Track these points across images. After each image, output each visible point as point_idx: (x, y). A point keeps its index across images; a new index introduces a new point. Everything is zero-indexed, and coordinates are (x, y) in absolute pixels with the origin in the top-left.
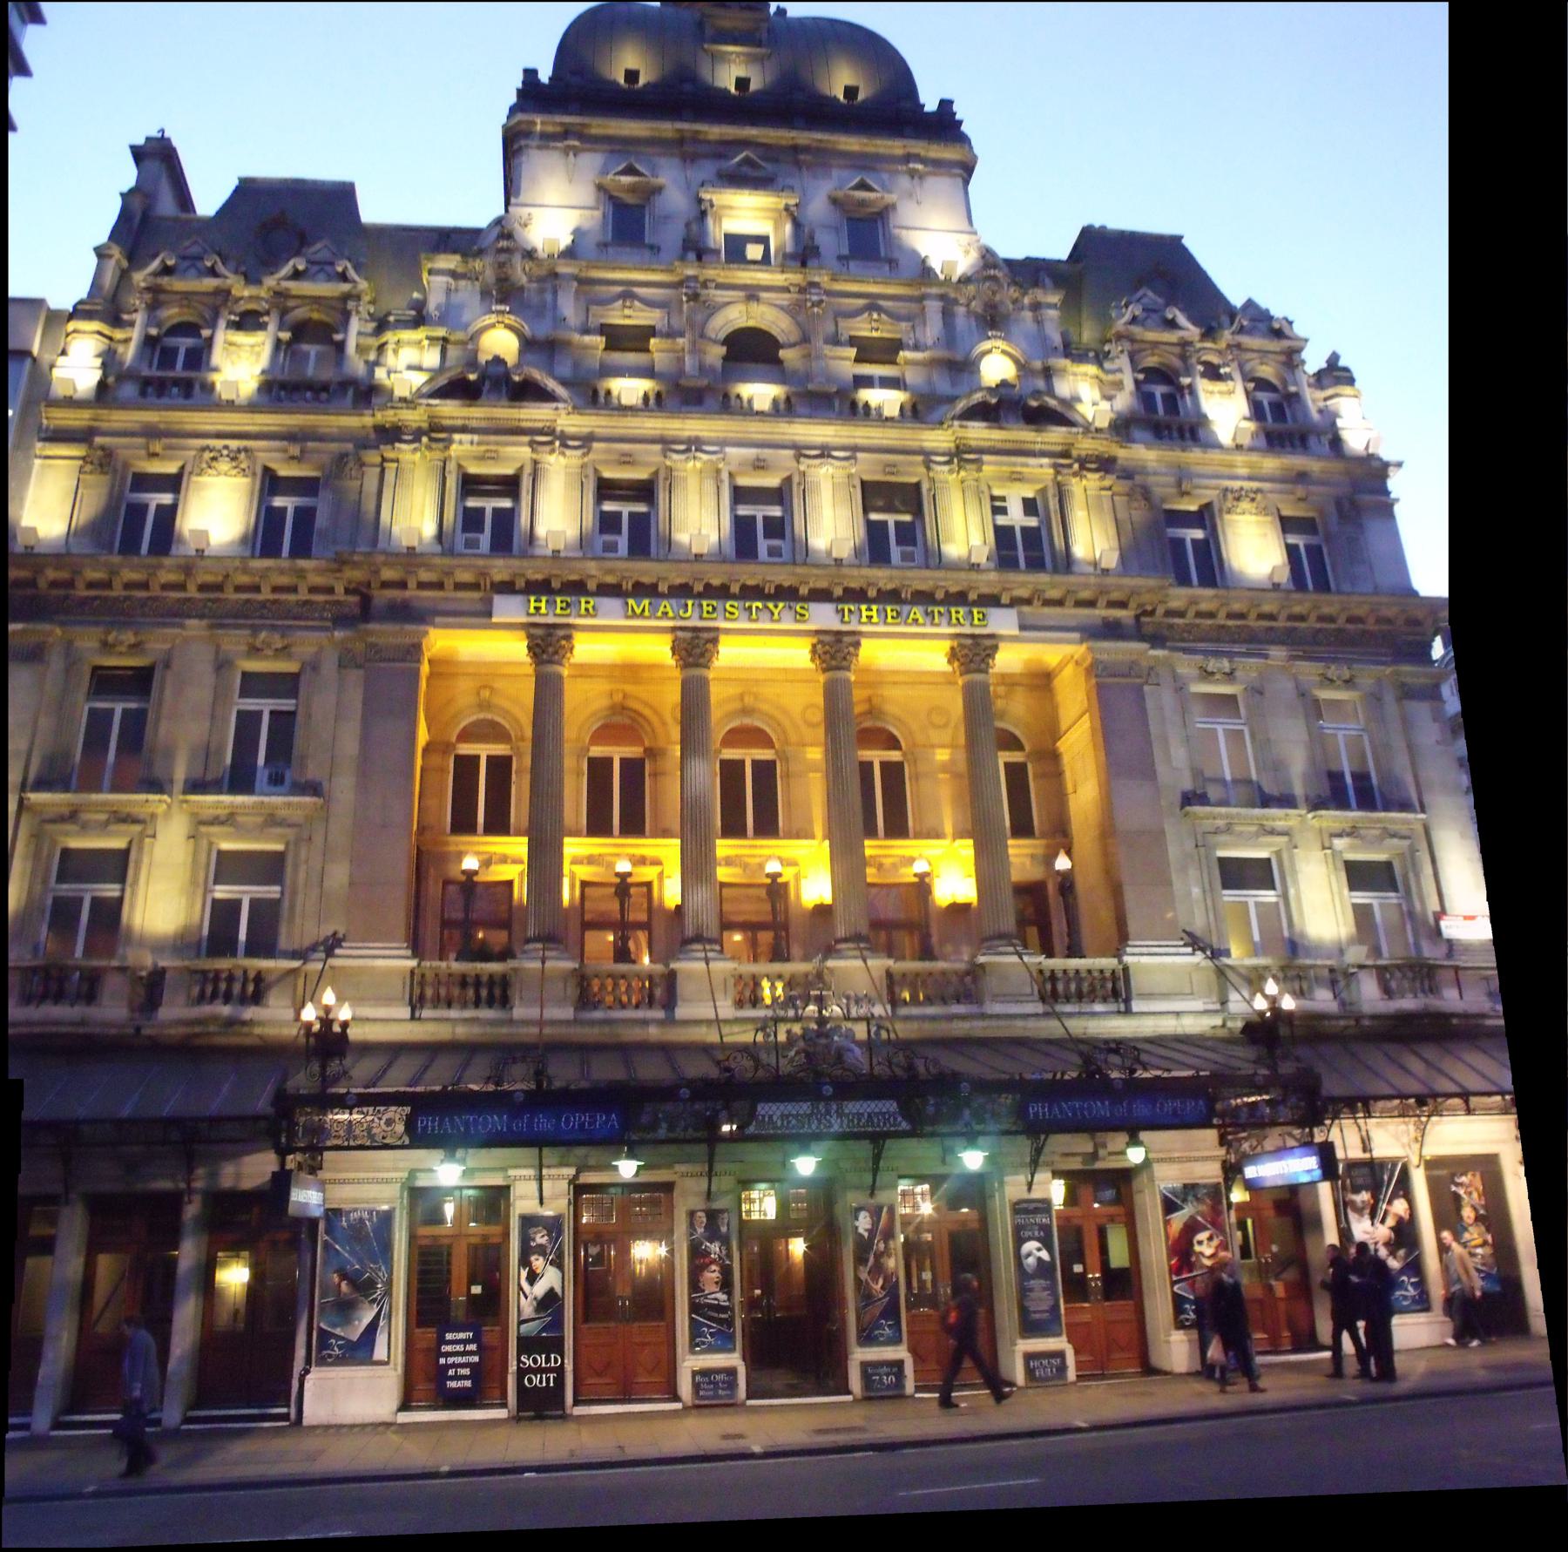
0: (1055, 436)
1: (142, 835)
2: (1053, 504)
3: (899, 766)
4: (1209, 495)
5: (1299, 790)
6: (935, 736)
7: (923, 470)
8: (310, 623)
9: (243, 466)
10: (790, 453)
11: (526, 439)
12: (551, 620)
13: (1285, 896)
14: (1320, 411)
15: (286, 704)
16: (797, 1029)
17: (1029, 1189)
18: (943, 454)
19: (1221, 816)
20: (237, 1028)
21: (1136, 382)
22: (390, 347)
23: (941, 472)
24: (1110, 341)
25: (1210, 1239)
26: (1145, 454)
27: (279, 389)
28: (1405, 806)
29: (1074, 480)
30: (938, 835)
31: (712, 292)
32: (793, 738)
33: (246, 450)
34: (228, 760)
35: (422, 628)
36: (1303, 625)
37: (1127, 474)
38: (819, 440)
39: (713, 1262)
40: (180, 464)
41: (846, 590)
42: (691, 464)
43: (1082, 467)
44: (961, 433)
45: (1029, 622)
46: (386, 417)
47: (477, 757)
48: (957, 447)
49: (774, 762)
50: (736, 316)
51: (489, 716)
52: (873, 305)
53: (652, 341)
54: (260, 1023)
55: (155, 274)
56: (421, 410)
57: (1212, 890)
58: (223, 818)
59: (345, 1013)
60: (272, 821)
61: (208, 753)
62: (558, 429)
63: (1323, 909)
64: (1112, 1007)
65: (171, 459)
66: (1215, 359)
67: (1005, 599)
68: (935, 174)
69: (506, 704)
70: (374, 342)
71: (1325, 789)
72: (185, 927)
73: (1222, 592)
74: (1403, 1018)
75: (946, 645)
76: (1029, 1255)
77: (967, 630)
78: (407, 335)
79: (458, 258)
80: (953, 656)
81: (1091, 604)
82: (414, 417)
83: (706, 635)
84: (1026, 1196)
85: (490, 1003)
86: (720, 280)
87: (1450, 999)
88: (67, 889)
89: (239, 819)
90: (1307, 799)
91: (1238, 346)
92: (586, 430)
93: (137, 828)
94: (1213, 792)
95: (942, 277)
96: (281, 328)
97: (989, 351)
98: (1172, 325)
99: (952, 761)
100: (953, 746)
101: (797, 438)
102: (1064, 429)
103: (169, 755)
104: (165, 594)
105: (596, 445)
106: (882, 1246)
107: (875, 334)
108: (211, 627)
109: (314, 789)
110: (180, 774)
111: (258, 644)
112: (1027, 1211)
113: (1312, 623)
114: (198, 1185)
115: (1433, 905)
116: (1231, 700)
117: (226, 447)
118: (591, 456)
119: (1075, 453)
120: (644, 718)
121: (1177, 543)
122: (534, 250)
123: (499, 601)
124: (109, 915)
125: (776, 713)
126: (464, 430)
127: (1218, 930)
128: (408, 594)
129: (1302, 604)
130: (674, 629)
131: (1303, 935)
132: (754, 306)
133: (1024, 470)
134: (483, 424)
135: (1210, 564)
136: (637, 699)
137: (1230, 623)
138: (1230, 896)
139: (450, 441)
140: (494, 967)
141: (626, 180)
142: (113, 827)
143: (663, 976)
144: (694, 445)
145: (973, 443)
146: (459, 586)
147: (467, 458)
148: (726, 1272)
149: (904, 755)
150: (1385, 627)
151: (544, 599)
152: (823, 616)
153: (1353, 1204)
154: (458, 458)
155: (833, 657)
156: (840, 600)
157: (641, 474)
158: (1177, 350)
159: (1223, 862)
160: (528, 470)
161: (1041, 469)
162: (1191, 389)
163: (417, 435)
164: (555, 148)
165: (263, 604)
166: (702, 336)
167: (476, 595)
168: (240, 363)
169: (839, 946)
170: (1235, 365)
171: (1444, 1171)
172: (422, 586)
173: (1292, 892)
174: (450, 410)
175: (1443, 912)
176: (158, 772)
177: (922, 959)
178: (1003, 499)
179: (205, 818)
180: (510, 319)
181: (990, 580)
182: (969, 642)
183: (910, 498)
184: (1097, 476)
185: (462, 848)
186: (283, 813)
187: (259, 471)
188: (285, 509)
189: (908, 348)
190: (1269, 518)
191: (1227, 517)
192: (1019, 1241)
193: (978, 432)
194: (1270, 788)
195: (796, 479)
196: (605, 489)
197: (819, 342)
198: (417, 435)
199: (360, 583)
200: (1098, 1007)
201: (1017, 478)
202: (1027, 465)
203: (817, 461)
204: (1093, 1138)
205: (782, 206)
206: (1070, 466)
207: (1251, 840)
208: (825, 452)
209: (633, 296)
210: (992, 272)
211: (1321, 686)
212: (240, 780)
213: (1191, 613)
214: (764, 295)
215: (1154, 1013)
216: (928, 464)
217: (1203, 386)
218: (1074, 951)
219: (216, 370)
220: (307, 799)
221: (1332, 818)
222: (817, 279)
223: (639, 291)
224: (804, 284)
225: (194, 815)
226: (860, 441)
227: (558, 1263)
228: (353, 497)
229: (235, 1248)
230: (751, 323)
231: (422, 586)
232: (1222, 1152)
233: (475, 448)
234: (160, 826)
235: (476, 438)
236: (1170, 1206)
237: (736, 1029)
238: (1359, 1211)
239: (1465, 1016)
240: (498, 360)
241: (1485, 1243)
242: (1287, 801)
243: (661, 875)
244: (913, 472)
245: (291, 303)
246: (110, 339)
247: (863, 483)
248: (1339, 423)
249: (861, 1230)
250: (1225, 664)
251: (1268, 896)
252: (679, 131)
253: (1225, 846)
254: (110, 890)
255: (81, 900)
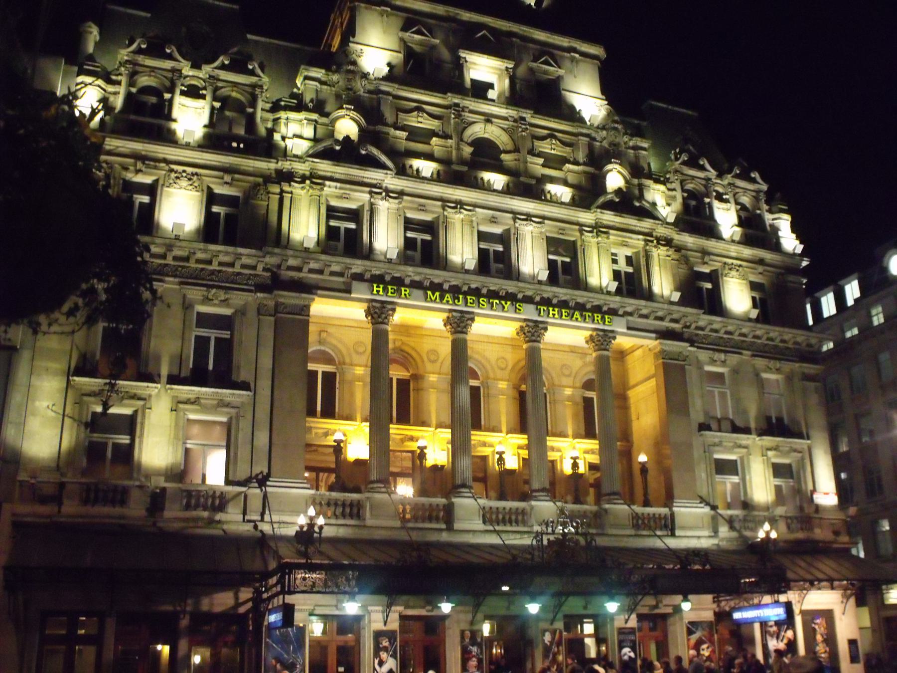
0: (646, 224)
1: (144, 408)
2: (643, 262)
3: (478, 388)
4: (717, 265)
5: (753, 425)
6: (565, 381)
7: (578, 234)
8: (204, 282)
9: (196, 184)
10: (510, 215)
11: (368, 189)
12: (384, 299)
13: (744, 480)
14: (771, 226)
15: (226, 334)
16: (552, 538)
17: (626, 622)
18: (589, 227)
19: (717, 437)
20: (214, 525)
21: (684, 198)
22: (283, 121)
23: (588, 237)
24: (670, 172)
25: (708, 648)
26: (688, 240)
27: (215, 140)
28: (800, 436)
29: (654, 250)
30: (565, 436)
31: (467, 114)
32: (491, 375)
33: (196, 174)
34: (191, 366)
35: (312, 296)
36: (759, 341)
37: (678, 249)
38: (525, 210)
39: (474, 656)
40: (154, 178)
41: (542, 298)
42: (458, 216)
43: (658, 243)
44: (600, 216)
45: (631, 325)
46: (286, 165)
47: (317, 372)
48: (596, 223)
49: (335, 373)
50: (478, 130)
51: (323, 348)
52: (552, 135)
53: (434, 139)
54: (227, 522)
55: (134, 52)
56: (307, 164)
57: (711, 475)
58: (192, 400)
59: (321, 521)
60: (223, 403)
61: (180, 360)
62: (384, 185)
63: (761, 487)
64: (665, 533)
65: (151, 174)
66: (721, 190)
67: (620, 312)
68: (584, 62)
69: (335, 342)
70: (271, 116)
71: (764, 425)
72: (173, 465)
73: (725, 320)
74: (798, 543)
75: (445, 315)
76: (625, 654)
77: (601, 327)
78: (293, 115)
79: (323, 71)
80: (447, 322)
81: (661, 319)
82: (301, 168)
83: (468, 316)
84: (384, 628)
85: (351, 516)
86: (471, 108)
87: (820, 534)
88: (97, 437)
89: (202, 401)
90: (756, 429)
91: (135, 64)
92: (400, 188)
93: (141, 403)
94: (714, 425)
95: (588, 123)
96: (215, 99)
97: (611, 170)
98: (702, 168)
99: (573, 395)
100: (573, 387)
101: (580, 220)
102: (652, 221)
103: (158, 359)
104: (152, 260)
105: (405, 198)
106: (556, 649)
107: (553, 152)
108: (181, 283)
109: (245, 386)
110: (164, 371)
111: (210, 297)
112: (624, 633)
113: (763, 341)
114: (188, 609)
115: (810, 487)
116: (720, 376)
117: (184, 171)
118: (404, 204)
119: (654, 234)
120: (411, 356)
121: (701, 292)
122: (368, 74)
123: (355, 284)
124: (126, 455)
125: (483, 361)
126: (331, 179)
127: (713, 497)
128: (301, 275)
129: (761, 330)
130: (450, 311)
131: (752, 500)
132: (489, 126)
133: (352, 193)
134: (343, 177)
135: (713, 303)
136: (408, 345)
137: (725, 336)
138: (718, 478)
139: (324, 185)
140: (355, 496)
141: (417, 37)
142: (126, 402)
143: (444, 506)
144: (459, 205)
145: (605, 222)
146: (332, 274)
147: (332, 196)
148: (480, 661)
149: (337, 368)
150: (797, 347)
151: (381, 286)
152: (529, 312)
153: (769, 632)
154: (327, 195)
155: (533, 335)
156: (537, 304)
157: (428, 217)
158: (703, 182)
159: (717, 461)
160: (367, 208)
161: (638, 242)
162: (171, 101)
163: (303, 179)
164: (376, 10)
165: (213, 272)
166: (462, 140)
167: (341, 279)
168: (190, 118)
169: (534, 494)
170: (210, 89)
171: (810, 616)
172: (311, 271)
173: (747, 477)
174: (325, 167)
175: (814, 490)
176: (151, 368)
177: (574, 503)
178: (615, 255)
179: (182, 399)
180: (354, 114)
181: (476, 282)
182: (601, 333)
183: (572, 249)
184: (665, 248)
185: (312, 425)
186: (228, 399)
187: (205, 189)
188: (219, 214)
189: (569, 162)
190: (744, 282)
191: (725, 278)
192: (621, 648)
193: (609, 217)
194: (739, 423)
195: (512, 231)
196: (409, 224)
197: (524, 152)
198: (303, 179)
199: (272, 265)
200: (645, 533)
201: (625, 245)
202: (631, 238)
203: (525, 223)
204: (656, 598)
205: (504, 68)
206: (380, 193)
207: (730, 450)
208: (528, 217)
209: (423, 110)
210: (616, 125)
211: (766, 372)
212: (198, 377)
213: (708, 329)
214: (494, 120)
215: (688, 537)
216: (581, 232)
217: (716, 204)
218: (646, 504)
219: (175, 120)
220: (244, 392)
221: (768, 441)
222: (524, 115)
223: (425, 108)
224: (516, 117)
225: (173, 397)
226: (546, 214)
227: (394, 656)
228: (263, 211)
229: (201, 644)
230: (486, 136)
231: (311, 271)
232: (715, 606)
233: (337, 191)
234: (153, 402)
235: (339, 185)
236: (690, 632)
237: (512, 536)
238: (772, 636)
239: (824, 542)
240: (347, 138)
241: (826, 652)
242: (746, 431)
243: (561, 457)
244: (572, 235)
245: (220, 84)
246: (104, 90)
247: (547, 237)
248: (780, 233)
249: (546, 642)
250: (722, 356)
251: (736, 479)
252: (447, 11)
253: (718, 452)
254: (124, 440)
255: (106, 444)
